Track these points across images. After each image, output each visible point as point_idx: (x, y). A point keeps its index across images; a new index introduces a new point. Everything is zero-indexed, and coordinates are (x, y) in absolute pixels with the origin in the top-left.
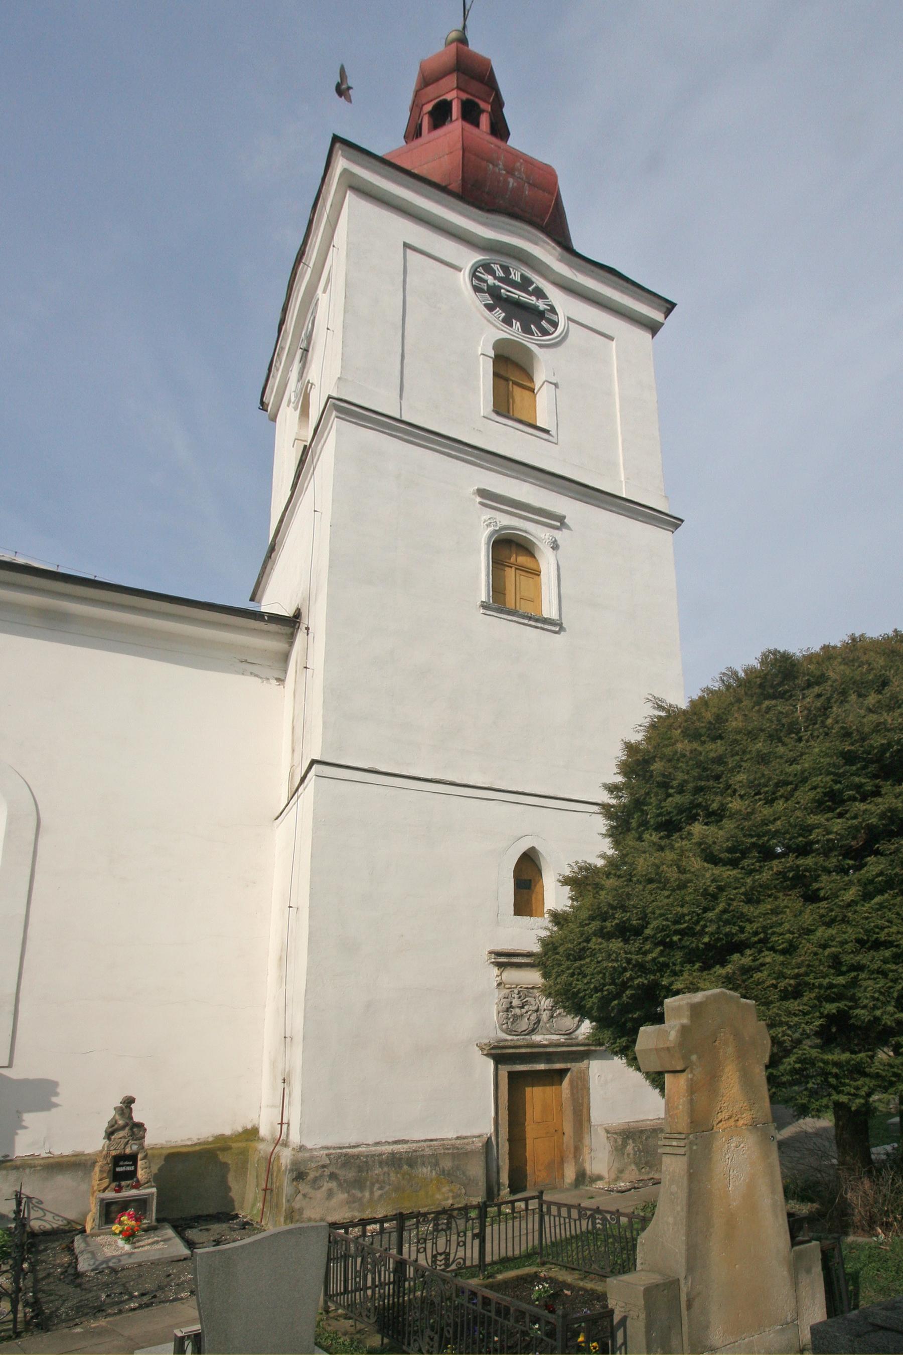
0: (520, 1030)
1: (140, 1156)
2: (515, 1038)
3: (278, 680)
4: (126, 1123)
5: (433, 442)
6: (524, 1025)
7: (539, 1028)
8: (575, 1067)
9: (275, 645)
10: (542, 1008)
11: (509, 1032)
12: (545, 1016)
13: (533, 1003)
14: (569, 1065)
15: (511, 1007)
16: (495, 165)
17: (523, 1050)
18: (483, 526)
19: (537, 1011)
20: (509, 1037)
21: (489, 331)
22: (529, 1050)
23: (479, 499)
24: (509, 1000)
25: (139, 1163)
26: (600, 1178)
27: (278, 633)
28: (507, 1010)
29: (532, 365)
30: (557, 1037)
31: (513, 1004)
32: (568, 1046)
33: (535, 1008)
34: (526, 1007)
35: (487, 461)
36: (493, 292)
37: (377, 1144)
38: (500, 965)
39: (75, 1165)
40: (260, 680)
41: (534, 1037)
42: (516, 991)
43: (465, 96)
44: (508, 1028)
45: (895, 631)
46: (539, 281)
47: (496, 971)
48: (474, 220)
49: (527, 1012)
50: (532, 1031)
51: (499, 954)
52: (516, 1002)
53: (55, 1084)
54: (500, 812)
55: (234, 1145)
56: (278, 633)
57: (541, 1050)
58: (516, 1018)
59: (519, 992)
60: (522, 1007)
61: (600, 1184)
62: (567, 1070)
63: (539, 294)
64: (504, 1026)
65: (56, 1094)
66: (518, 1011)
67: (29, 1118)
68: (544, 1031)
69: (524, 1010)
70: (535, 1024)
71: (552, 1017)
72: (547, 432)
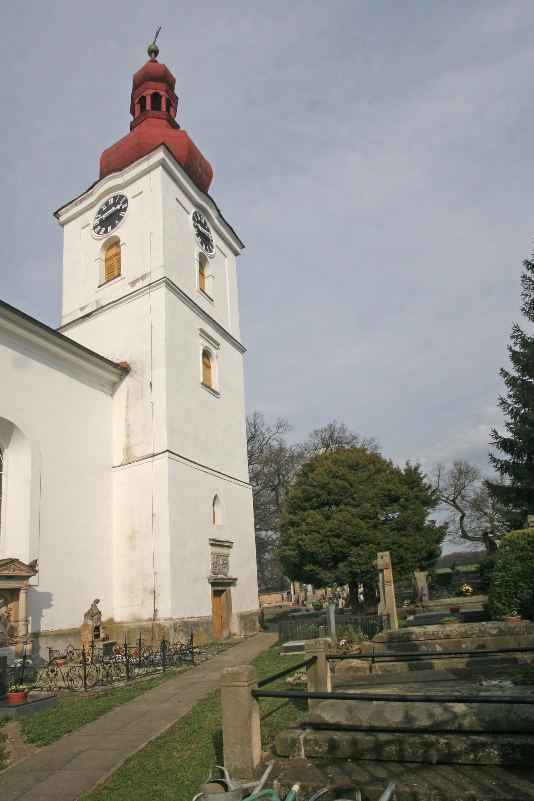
1: (100, 627)
3: (111, 395)
4: (94, 613)
5: (196, 309)
8: (228, 589)
9: (114, 378)
14: (224, 588)
16: (197, 161)
17: (220, 581)
18: (201, 344)
21: (198, 248)
23: (199, 332)
25: (101, 630)
26: (235, 634)
27: (117, 374)
29: (205, 264)
35: (201, 314)
36: (199, 230)
37: (188, 618)
38: (212, 545)
39: (75, 633)
40: (105, 395)
43: (168, 97)
46: (209, 225)
47: (210, 547)
48: (196, 192)
51: (213, 540)
54: (209, 478)
55: (108, 626)
56: (117, 374)
61: (235, 637)
62: (225, 590)
63: (208, 230)
65: (52, 600)
67: (44, 611)
72: (212, 301)
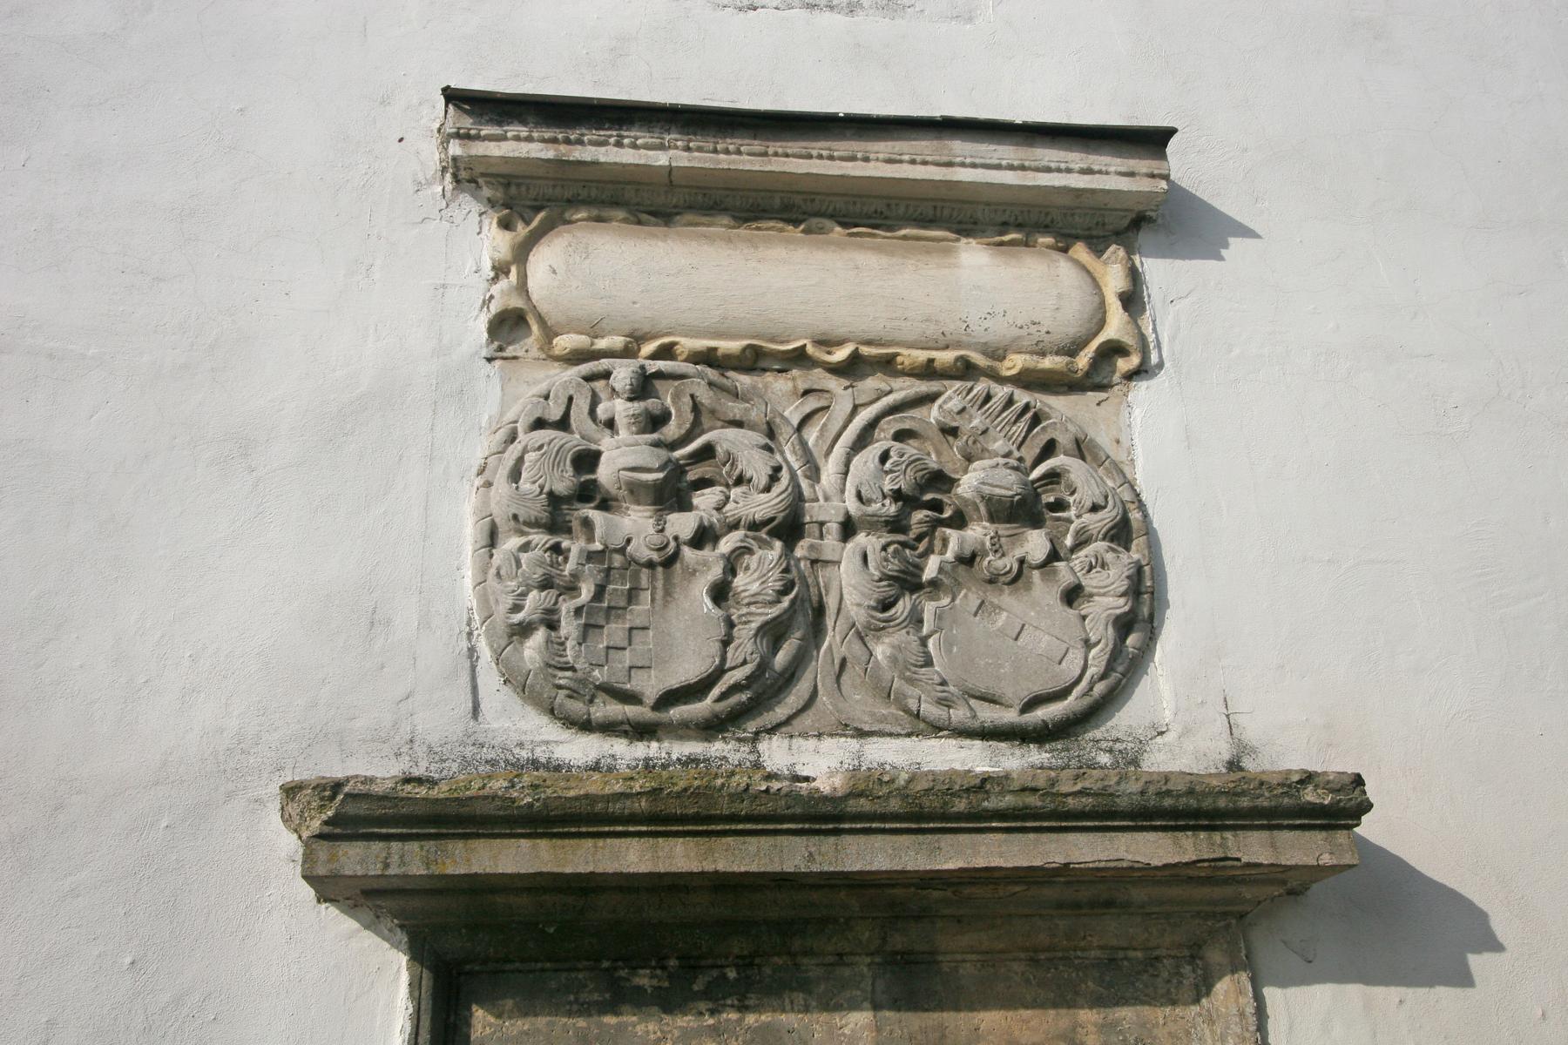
0: (651, 686)
2: (626, 752)
6: (682, 639)
7: (819, 668)
10: (826, 508)
11: (572, 700)
12: (850, 578)
13: (756, 465)
15: (587, 493)
17: (633, 856)
19: (789, 528)
20: (578, 749)
22: (681, 856)
24: (573, 441)
28: (556, 515)
30: (974, 758)
31: (605, 473)
32: (1019, 820)
33: (762, 505)
34: (705, 500)
38: (459, 120)
41: (777, 754)
42: (623, 374)
44: (555, 663)
45: (1464, 979)
49: (704, 537)
50: (757, 700)
52: (623, 456)
53: (1492, 944)
57: (792, 855)
58: (623, 581)
59: (644, 386)
60: (670, 493)
64: (533, 648)
66: (635, 525)
68: (860, 704)
69: (682, 524)
70: (774, 633)
71: (908, 581)
